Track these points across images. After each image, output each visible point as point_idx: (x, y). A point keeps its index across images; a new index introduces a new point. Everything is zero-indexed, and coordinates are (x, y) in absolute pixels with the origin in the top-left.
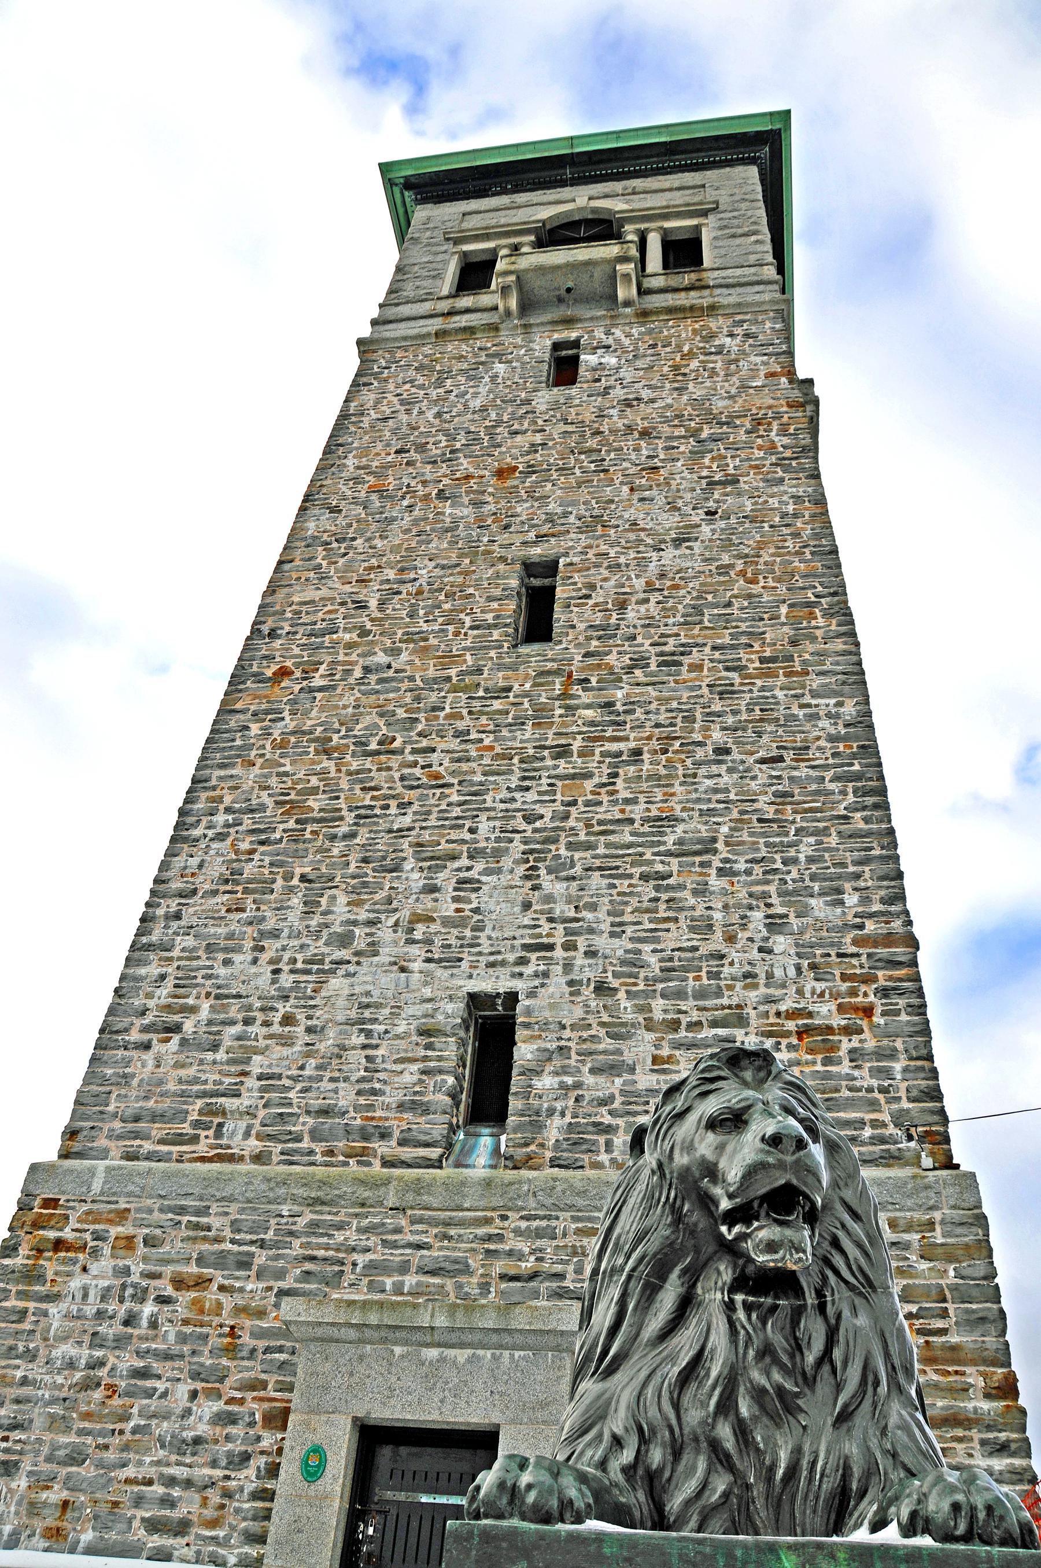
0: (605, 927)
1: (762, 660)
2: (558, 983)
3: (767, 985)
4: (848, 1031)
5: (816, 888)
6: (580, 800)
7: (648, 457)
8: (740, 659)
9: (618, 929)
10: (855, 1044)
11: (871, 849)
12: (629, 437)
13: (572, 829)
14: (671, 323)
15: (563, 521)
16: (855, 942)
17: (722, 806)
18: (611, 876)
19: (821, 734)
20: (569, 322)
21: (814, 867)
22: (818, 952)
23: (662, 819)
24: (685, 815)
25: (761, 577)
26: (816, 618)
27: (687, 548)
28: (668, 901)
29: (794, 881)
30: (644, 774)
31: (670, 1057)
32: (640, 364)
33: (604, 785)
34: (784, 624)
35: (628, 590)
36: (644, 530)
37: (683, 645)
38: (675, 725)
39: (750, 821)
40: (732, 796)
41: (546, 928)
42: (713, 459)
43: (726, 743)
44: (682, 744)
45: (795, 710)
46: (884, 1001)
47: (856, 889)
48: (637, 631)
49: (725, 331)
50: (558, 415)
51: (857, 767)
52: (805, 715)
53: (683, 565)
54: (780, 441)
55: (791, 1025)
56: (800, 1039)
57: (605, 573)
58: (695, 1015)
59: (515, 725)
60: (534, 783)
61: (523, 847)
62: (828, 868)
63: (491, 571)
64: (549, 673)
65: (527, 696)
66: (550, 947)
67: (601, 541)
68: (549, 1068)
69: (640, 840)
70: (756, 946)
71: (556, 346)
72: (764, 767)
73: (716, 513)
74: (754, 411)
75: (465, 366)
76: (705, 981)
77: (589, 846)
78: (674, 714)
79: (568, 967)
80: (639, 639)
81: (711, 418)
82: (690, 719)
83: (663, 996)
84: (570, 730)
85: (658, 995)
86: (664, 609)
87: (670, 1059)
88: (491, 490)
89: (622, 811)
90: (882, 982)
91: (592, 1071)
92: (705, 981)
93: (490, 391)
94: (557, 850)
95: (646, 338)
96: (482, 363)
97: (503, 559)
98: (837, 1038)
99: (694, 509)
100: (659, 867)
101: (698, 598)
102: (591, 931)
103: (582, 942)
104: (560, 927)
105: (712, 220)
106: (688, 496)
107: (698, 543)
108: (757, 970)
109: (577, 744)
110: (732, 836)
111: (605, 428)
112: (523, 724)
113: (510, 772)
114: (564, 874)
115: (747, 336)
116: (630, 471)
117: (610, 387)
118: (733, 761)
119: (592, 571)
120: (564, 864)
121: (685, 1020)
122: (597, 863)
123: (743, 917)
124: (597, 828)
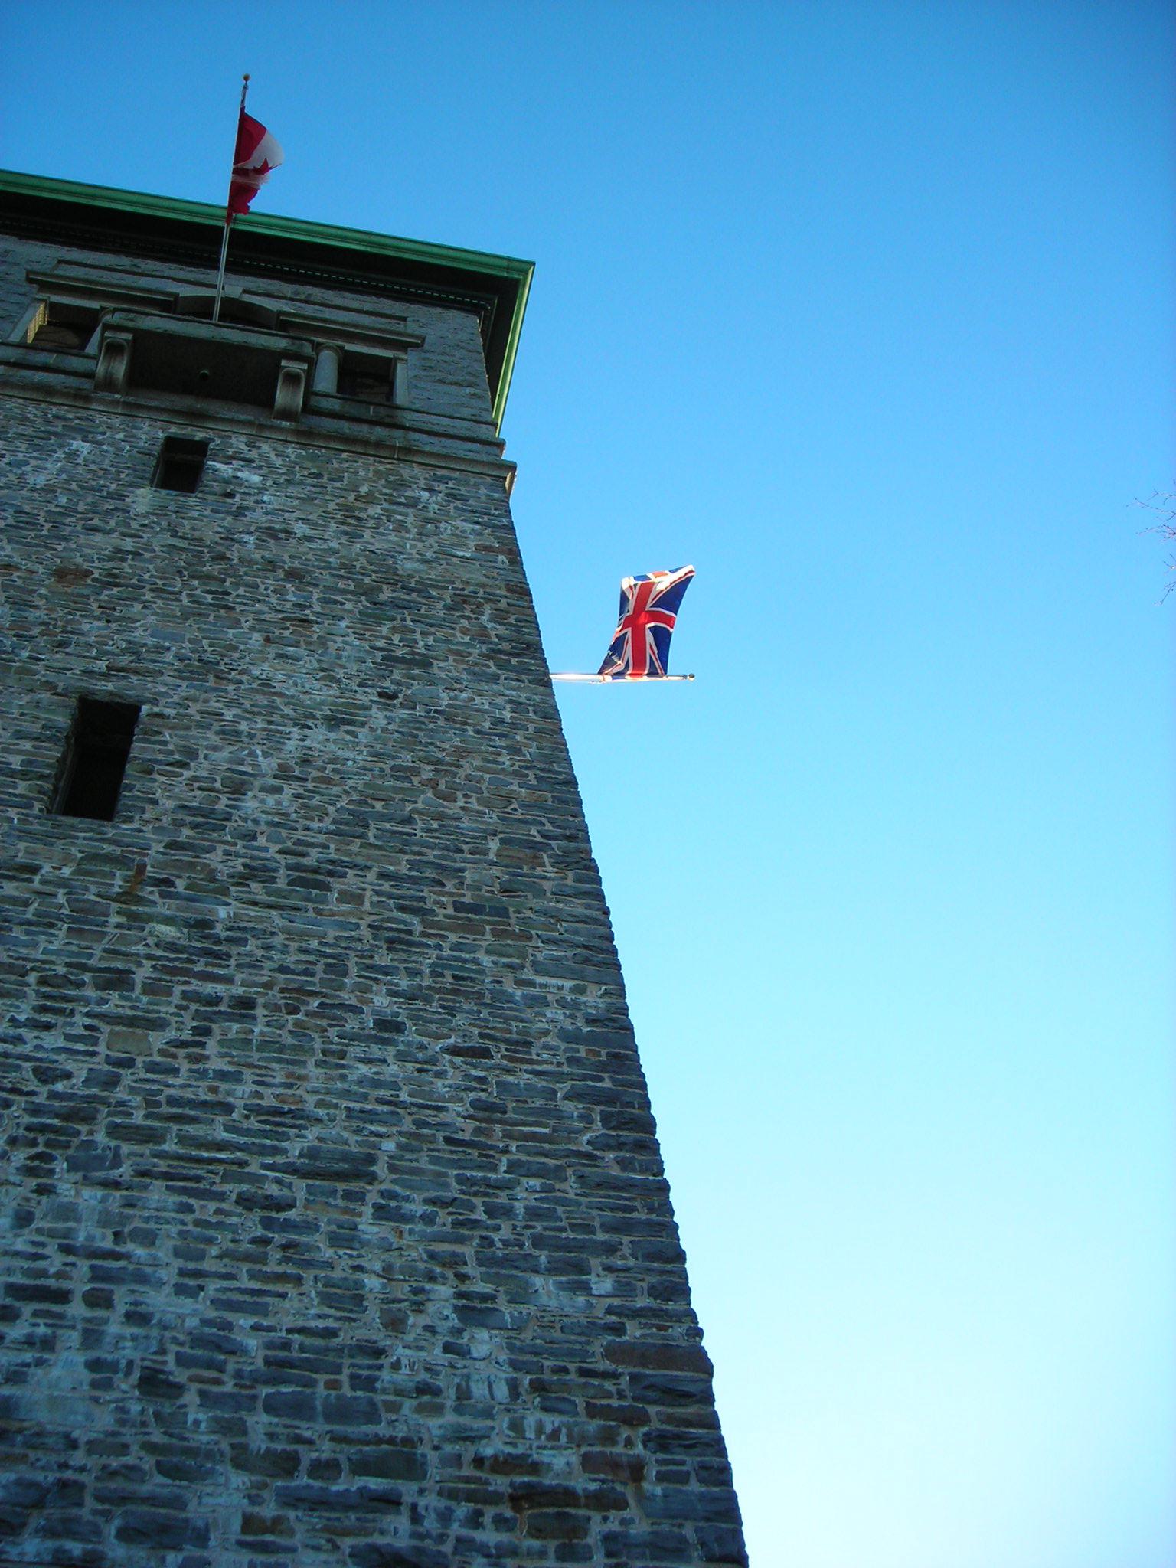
0: (169, 1275)
1: (458, 907)
2: (68, 1367)
3: (458, 1410)
4: (605, 1501)
5: (543, 1259)
6: (140, 1061)
7: (296, 605)
8: (422, 899)
9: (192, 1282)
10: (613, 1526)
11: (632, 1209)
12: (269, 574)
13: (121, 1103)
14: (344, 455)
15: (153, 656)
16: (610, 1353)
17: (386, 1108)
18: (184, 1191)
19: (550, 1027)
20: (196, 417)
21: (539, 1226)
22: (547, 1363)
23: (282, 1113)
24: (322, 1112)
25: (459, 794)
26: (543, 865)
27: (347, 732)
28: (285, 1247)
29: (506, 1243)
30: (256, 1037)
31: (277, 1521)
32: (293, 490)
33: (183, 1044)
34: (492, 864)
35: (249, 770)
36: (281, 695)
37: (332, 862)
38: (313, 975)
39: (432, 1139)
40: (404, 1096)
41: (56, 1262)
42: (394, 630)
43: (398, 1014)
44: (322, 1005)
45: (509, 987)
46: (661, 1456)
47: (609, 1269)
48: (259, 829)
49: (422, 483)
50: (164, 524)
51: (607, 1084)
52: (524, 996)
53: (340, 753)
54: (496, 630)
55: (500, 1483)
56: (517, 1508)
57: (215, 740)
58: (326, 1450)
59: (38, 924)
60: (61, 1019)
61: (27, 1119)
62: (563, 1229)
63: (26, 698)
64: (109, 859)
65: (64, 886)
66: (63, 1297)
67: (212, 696)
68: (37, 1520)
69: (242, 1140)
70: (440, 1340)
71: (171, 443)
72: (458, 1060)
73: (394, 696)
74: (458, 585)
75: (30, 431)
76: (347, 1391)
77: (149, 1136)
78: (312, 958)
79: (92, 1336)
80: (262, 841)
81: (393, 578)
82: (338, 969)
83: (269, 1409)
84: (134, 949)
85: (260, 1405)
86: (304, 806)
87: (276, 1525)
88: (43, 591)
89: (214, 1090)
90: (656, 1424)
91: (124, 1535)
92: (347, 1391)
93: (62, 470)
94: (91, 1133)
95: (307, 464)
96: (55, 434)
97: (50, 687)
98: (581, 1512)
99: (360, 685)
100: (273, 1190)
101: (359, 802)
102: (142, 1278)
103: (122, 1298)
104: (84, 1266)
105: (411, 356)
106: (354, 668)
107: (365, 730)
108: (441, 1383)
109: (142, 973)
110: (401, 1158)
111: (234, 554)
112: (52, 925)
113: (23, 996)
114: (99, 1174)
115: (452, 496)
116: (267, 617)
117: (247, 508)
118: (409, 1044)
119: (193, 732)
120: (101, 1159)
121: (307, 1456)
122: (162, 1166)
123: (416, 1291)
124: (165, 1109)
